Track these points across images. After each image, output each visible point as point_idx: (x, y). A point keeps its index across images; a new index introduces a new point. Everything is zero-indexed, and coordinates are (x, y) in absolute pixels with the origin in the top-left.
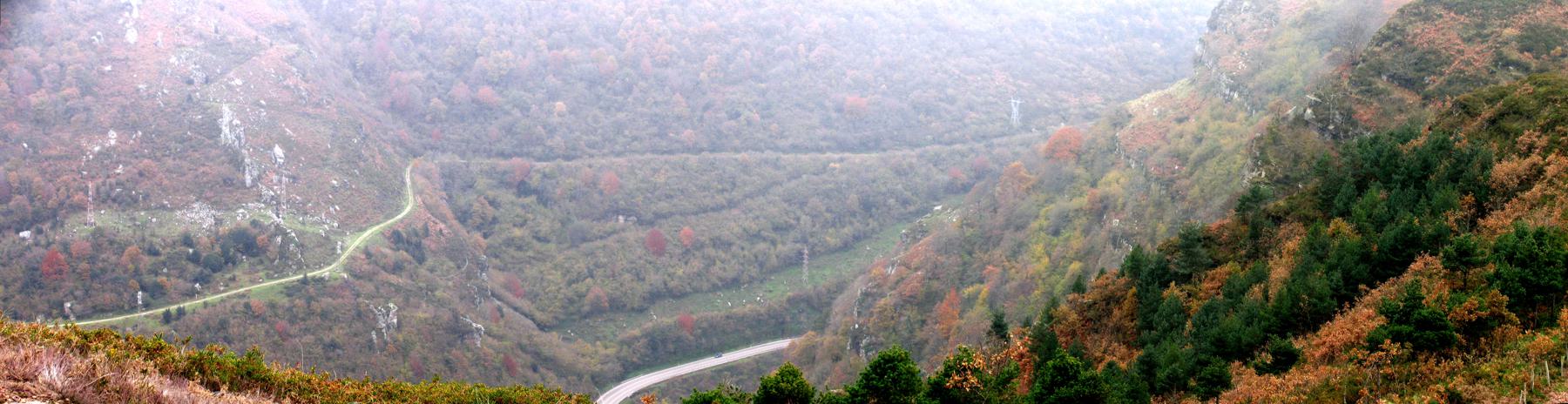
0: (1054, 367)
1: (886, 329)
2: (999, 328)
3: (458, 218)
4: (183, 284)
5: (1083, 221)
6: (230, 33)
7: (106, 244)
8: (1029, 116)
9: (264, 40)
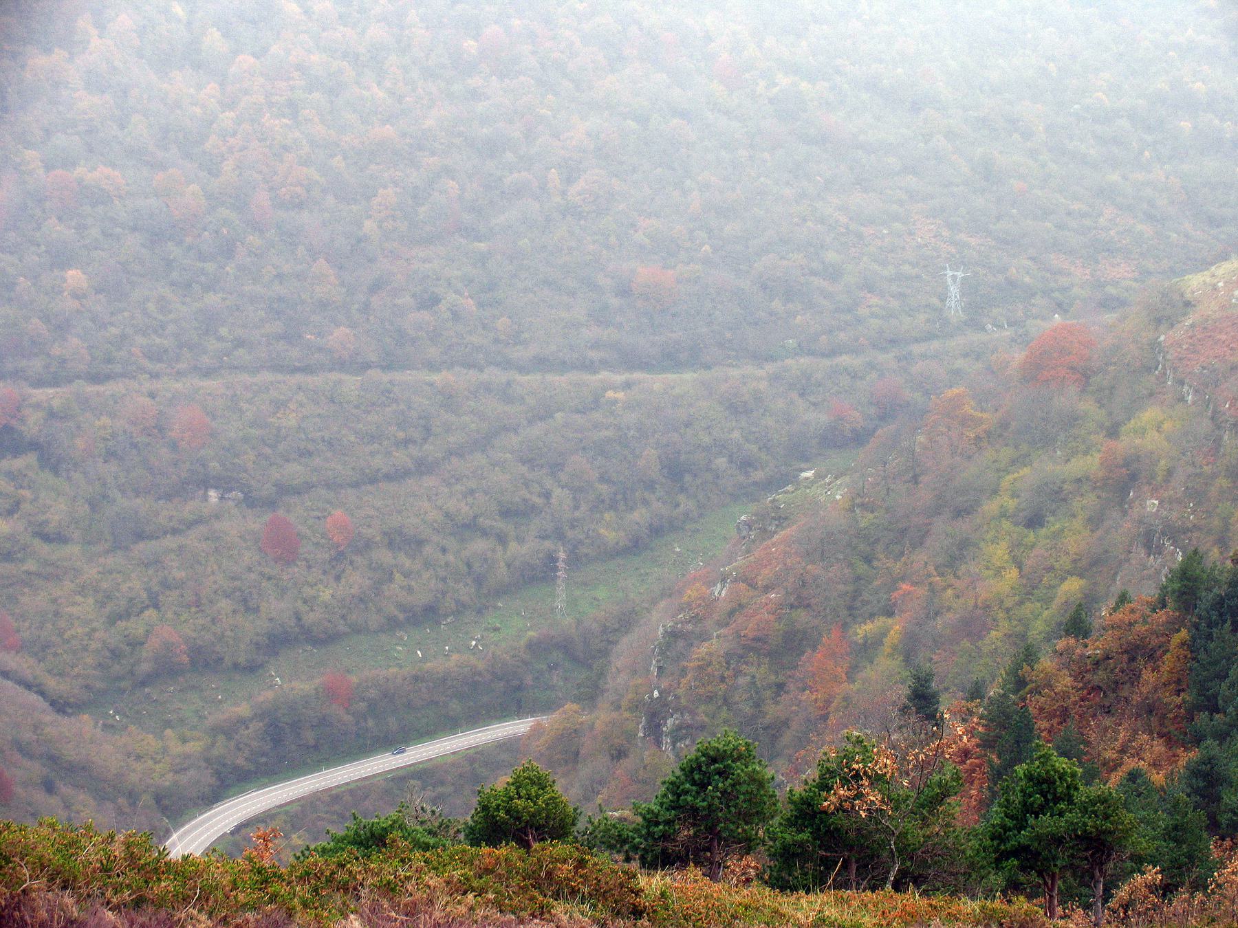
0: (1030, 777)
1: (710, 699)
2: (923, 701)
5: (1088, 501)
8: (978, 306)
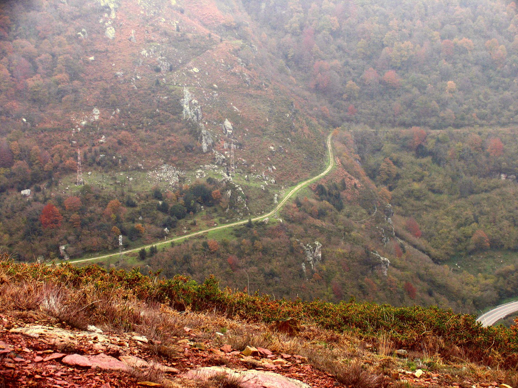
3: (369, 175)
4: (155, 229)
6: (189, 31)
7: (93, 199)
9: (216, 37)
